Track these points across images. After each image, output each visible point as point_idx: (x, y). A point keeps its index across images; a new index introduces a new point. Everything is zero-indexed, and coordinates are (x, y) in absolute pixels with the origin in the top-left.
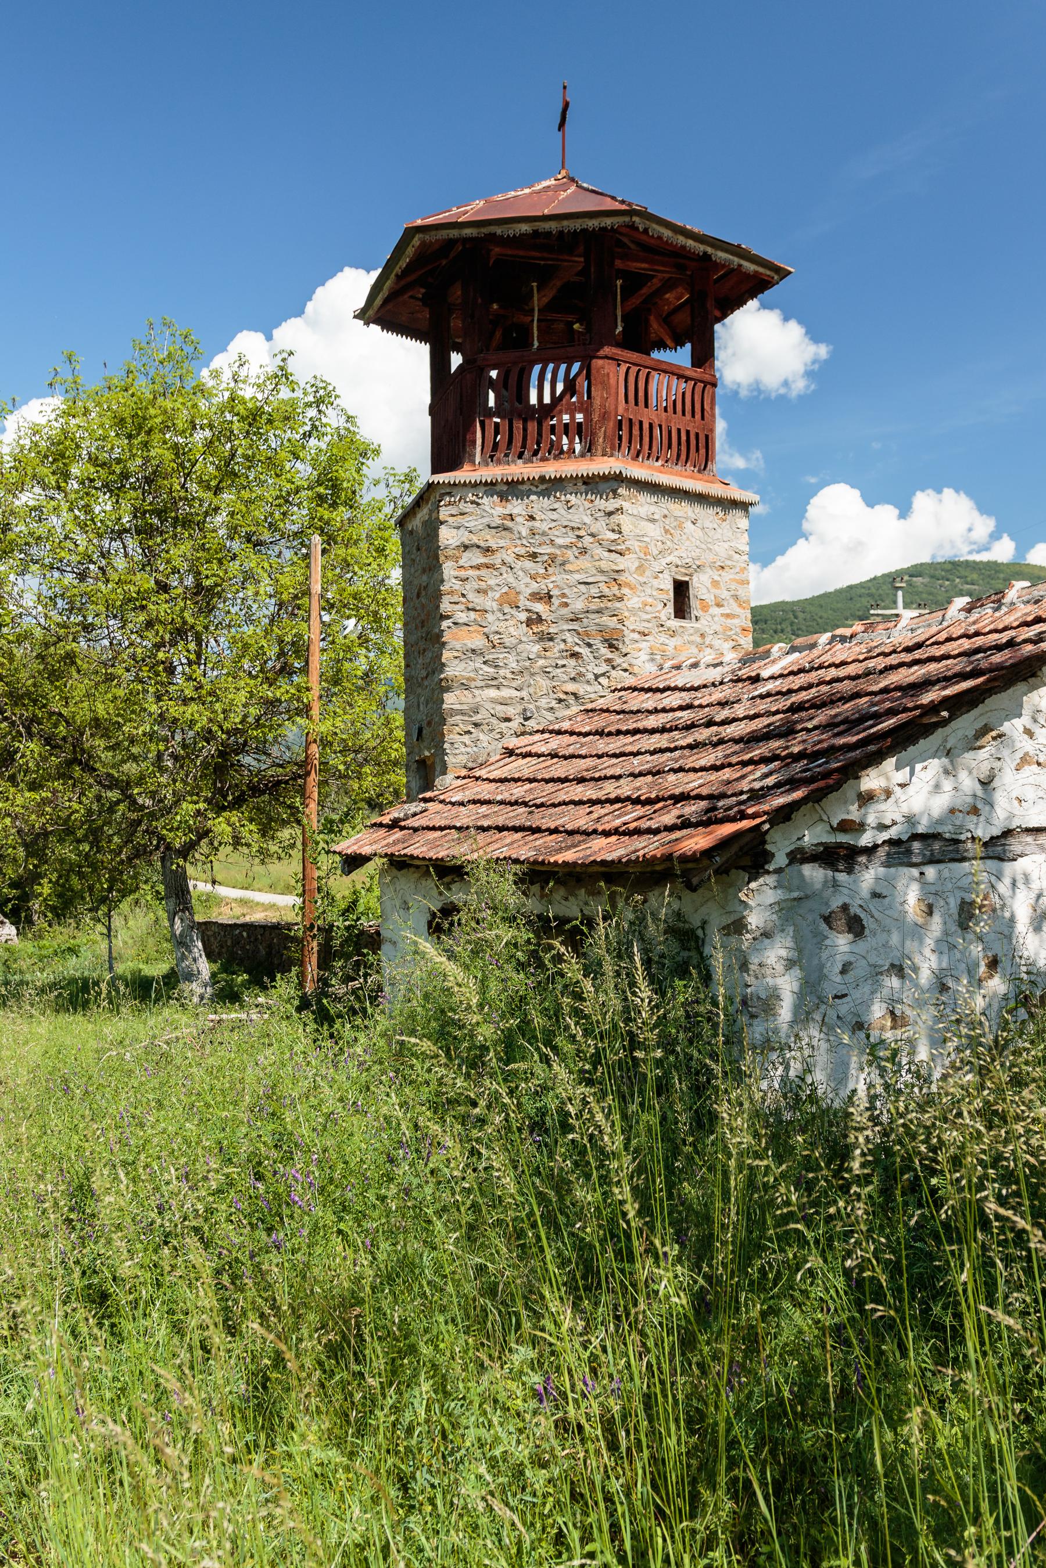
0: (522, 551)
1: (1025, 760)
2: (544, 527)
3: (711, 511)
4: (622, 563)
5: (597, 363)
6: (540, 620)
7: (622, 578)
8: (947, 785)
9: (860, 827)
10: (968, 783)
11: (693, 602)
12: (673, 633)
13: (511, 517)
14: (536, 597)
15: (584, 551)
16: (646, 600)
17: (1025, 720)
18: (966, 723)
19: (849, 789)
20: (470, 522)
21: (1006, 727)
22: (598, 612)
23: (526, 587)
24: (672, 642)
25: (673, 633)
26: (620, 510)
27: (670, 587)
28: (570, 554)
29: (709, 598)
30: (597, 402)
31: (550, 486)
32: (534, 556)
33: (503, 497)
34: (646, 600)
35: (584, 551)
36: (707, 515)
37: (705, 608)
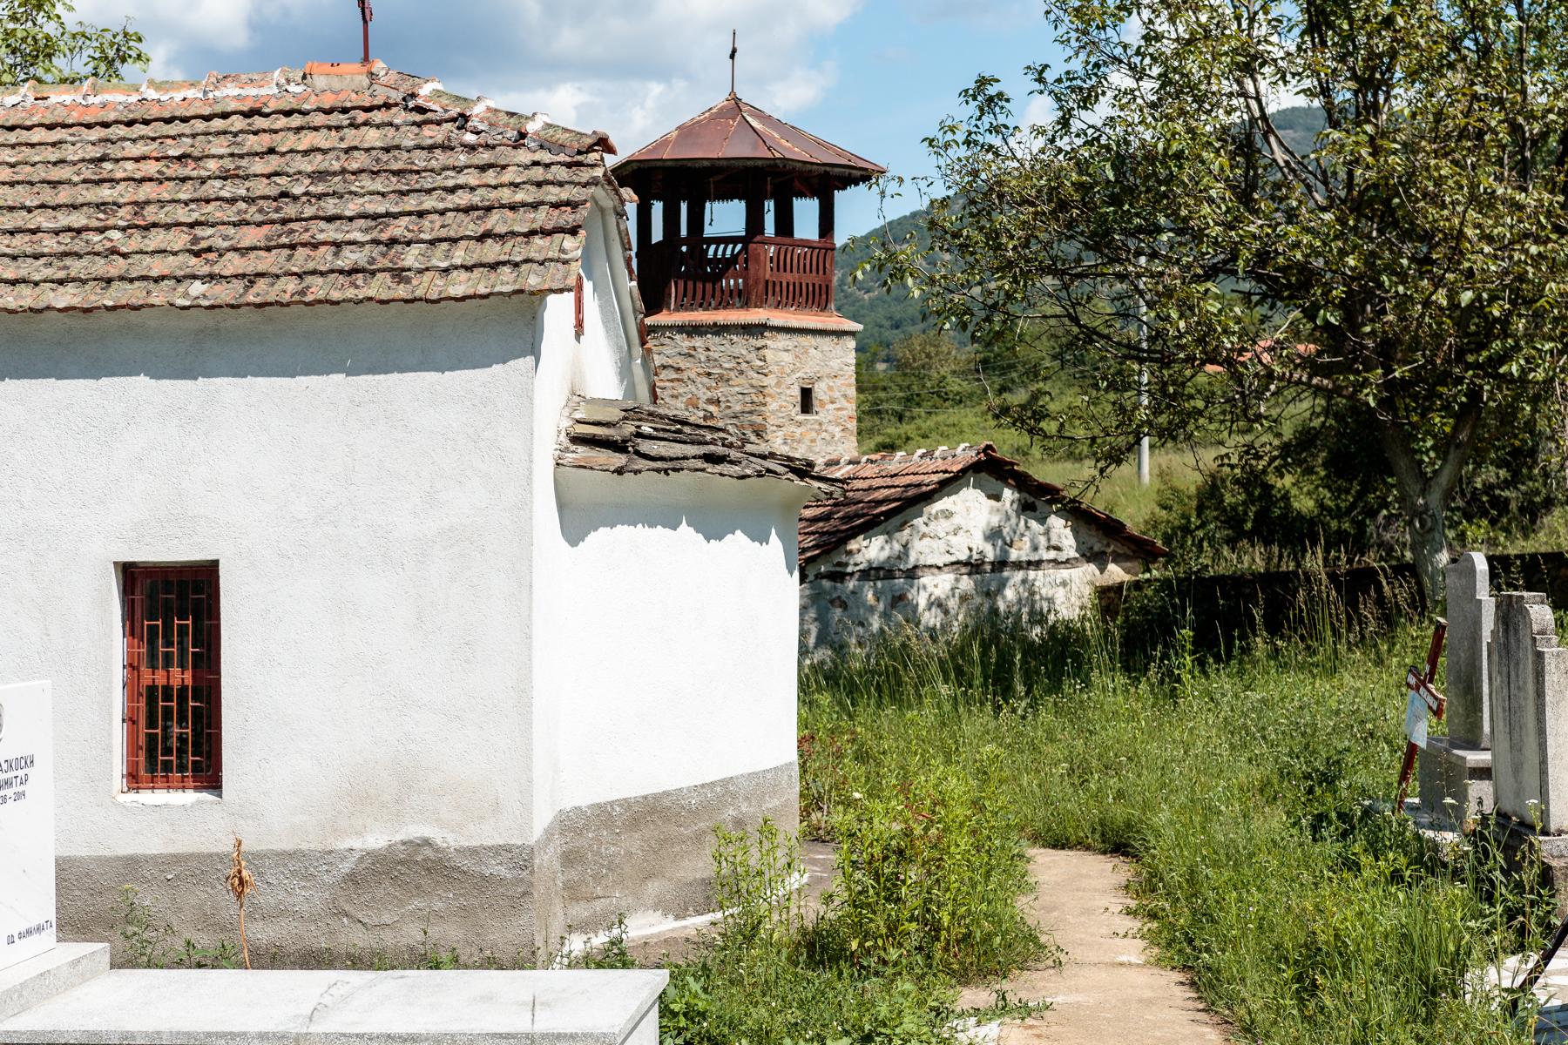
0: (701, 371)
1: (924, 536)
2: (716, 355)
3: (828, 339)
4: (766, 381)
5: (752, 246)
6: (712, 416)
7: (766, 391)
8: (887, 547)
9: (847, 565)
10: (897, 547)
11: (815, 402)
12: (800, 424)
13: (695, 348)
14: (710, 401)
15: (741, 373)
16: (782, 402)
17: (924, 518)
18: (896, 520)
19: (842, 549)
20: (667, 350)
21: (915, 522)
22: (751, 412)
23: (704, 394)
24: (799, 431)
25: (800, 424)
26: (765, 346)
27: (797, 392)
28: (732, 374)
29: (826, 398)
30: (752, 271)
31: (719, 329)
32: (709, 374)
33: (690, 335)
34: (782, 402)
35: (741, 373)
36: (825, 343)
37: (823, 404)
